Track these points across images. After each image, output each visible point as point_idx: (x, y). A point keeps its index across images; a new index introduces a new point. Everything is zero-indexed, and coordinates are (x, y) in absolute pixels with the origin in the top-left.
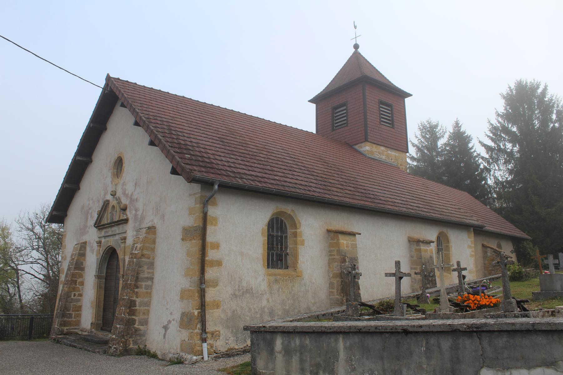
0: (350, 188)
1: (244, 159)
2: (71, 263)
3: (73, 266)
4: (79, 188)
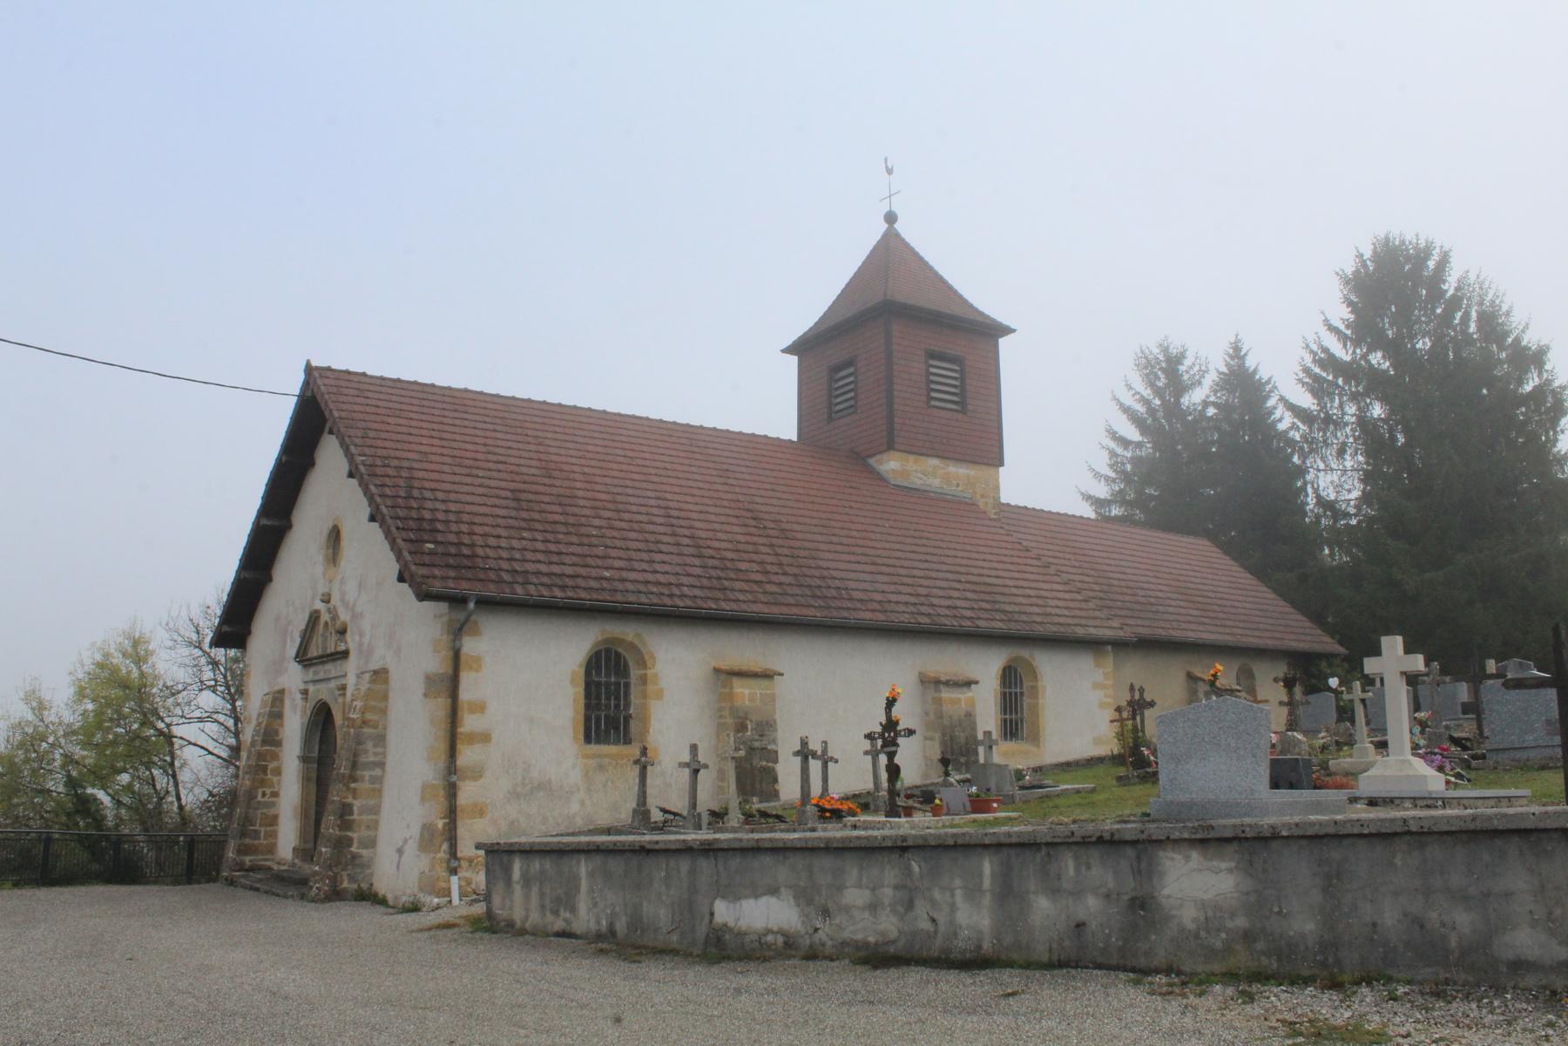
3: (259, 739)
4: (269, 579)
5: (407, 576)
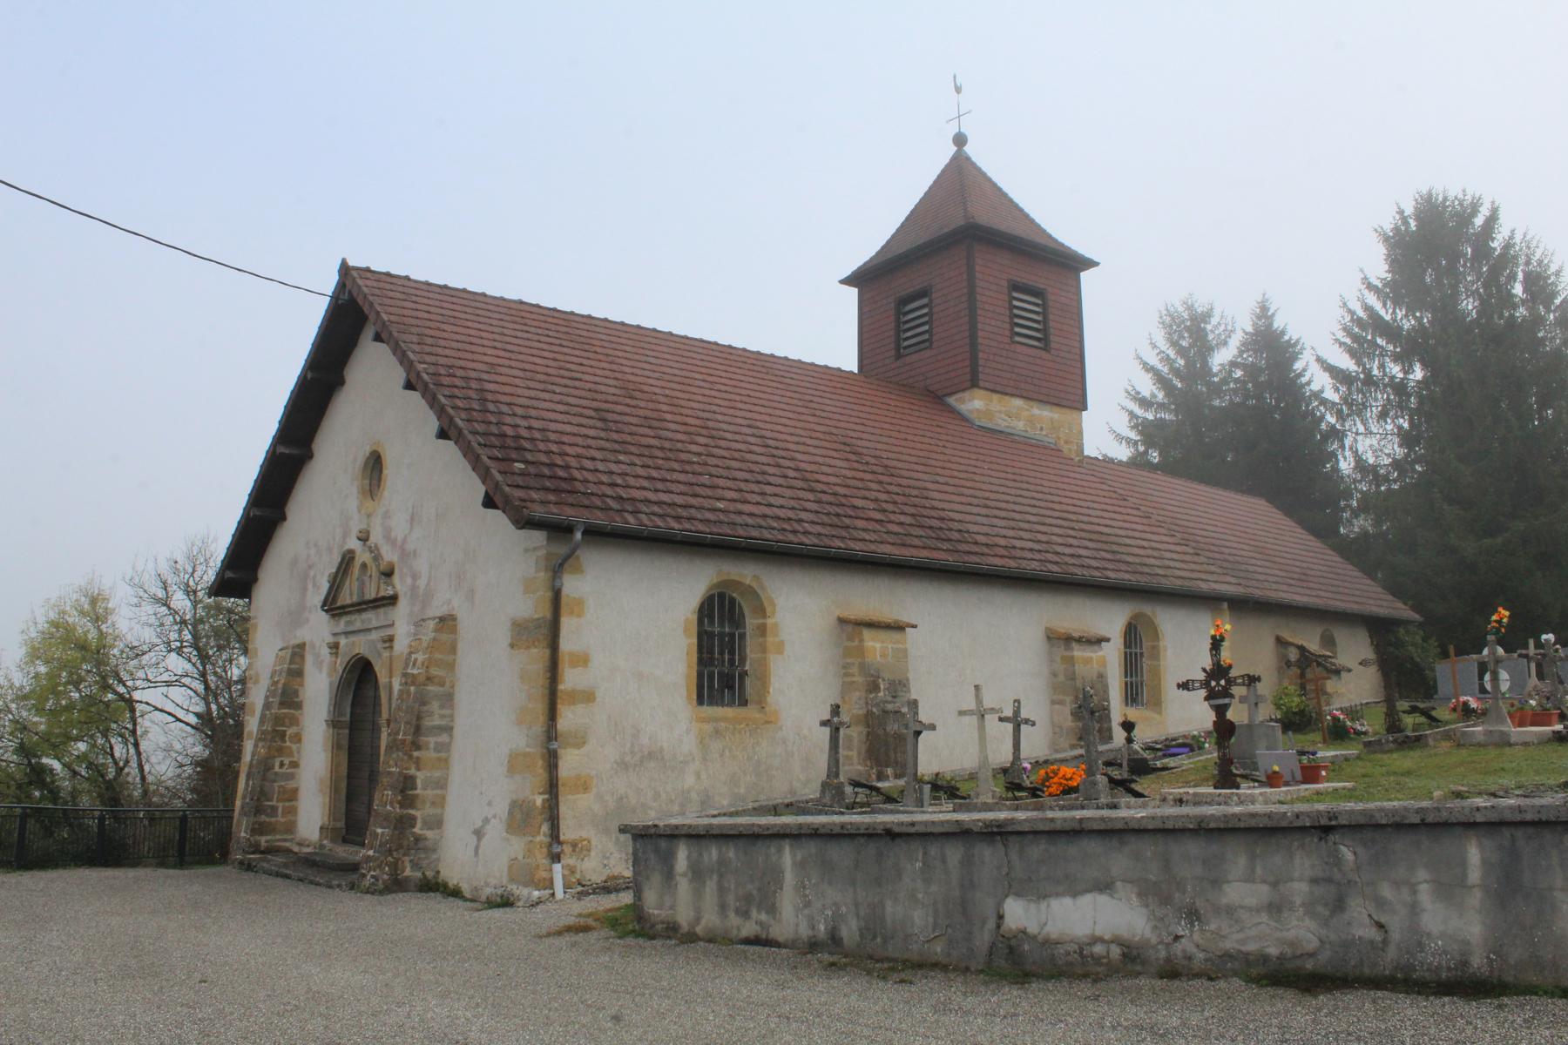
0: (902, 518)
2: (271, 692)
3: (276, 700)
4: (283, 518)
5: (498, 499)
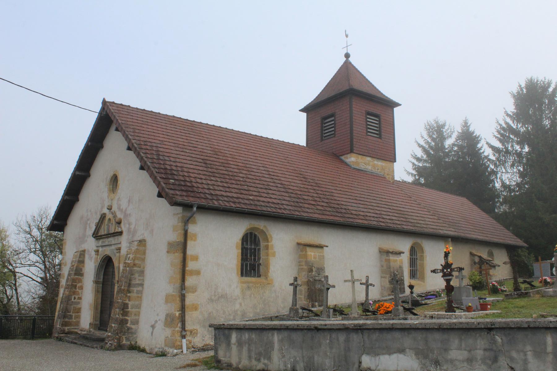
0: (323, 204)
1: (223, 180)
2: (71, 269)
3: (73, 272)
5: (163, 194)
